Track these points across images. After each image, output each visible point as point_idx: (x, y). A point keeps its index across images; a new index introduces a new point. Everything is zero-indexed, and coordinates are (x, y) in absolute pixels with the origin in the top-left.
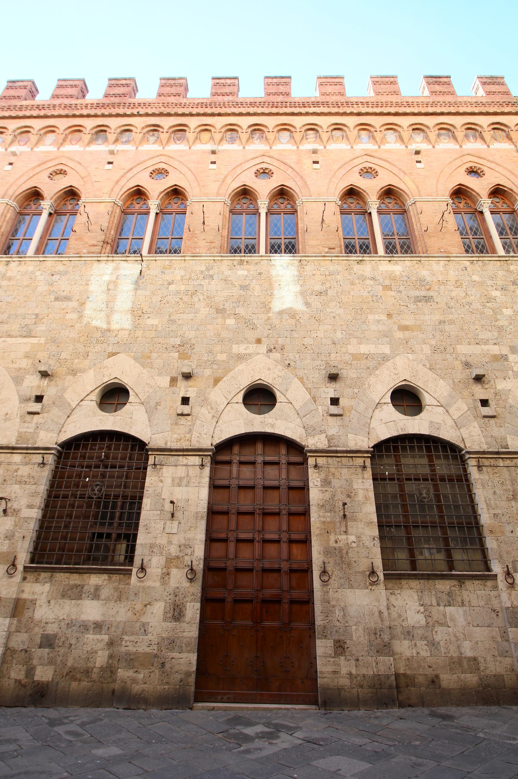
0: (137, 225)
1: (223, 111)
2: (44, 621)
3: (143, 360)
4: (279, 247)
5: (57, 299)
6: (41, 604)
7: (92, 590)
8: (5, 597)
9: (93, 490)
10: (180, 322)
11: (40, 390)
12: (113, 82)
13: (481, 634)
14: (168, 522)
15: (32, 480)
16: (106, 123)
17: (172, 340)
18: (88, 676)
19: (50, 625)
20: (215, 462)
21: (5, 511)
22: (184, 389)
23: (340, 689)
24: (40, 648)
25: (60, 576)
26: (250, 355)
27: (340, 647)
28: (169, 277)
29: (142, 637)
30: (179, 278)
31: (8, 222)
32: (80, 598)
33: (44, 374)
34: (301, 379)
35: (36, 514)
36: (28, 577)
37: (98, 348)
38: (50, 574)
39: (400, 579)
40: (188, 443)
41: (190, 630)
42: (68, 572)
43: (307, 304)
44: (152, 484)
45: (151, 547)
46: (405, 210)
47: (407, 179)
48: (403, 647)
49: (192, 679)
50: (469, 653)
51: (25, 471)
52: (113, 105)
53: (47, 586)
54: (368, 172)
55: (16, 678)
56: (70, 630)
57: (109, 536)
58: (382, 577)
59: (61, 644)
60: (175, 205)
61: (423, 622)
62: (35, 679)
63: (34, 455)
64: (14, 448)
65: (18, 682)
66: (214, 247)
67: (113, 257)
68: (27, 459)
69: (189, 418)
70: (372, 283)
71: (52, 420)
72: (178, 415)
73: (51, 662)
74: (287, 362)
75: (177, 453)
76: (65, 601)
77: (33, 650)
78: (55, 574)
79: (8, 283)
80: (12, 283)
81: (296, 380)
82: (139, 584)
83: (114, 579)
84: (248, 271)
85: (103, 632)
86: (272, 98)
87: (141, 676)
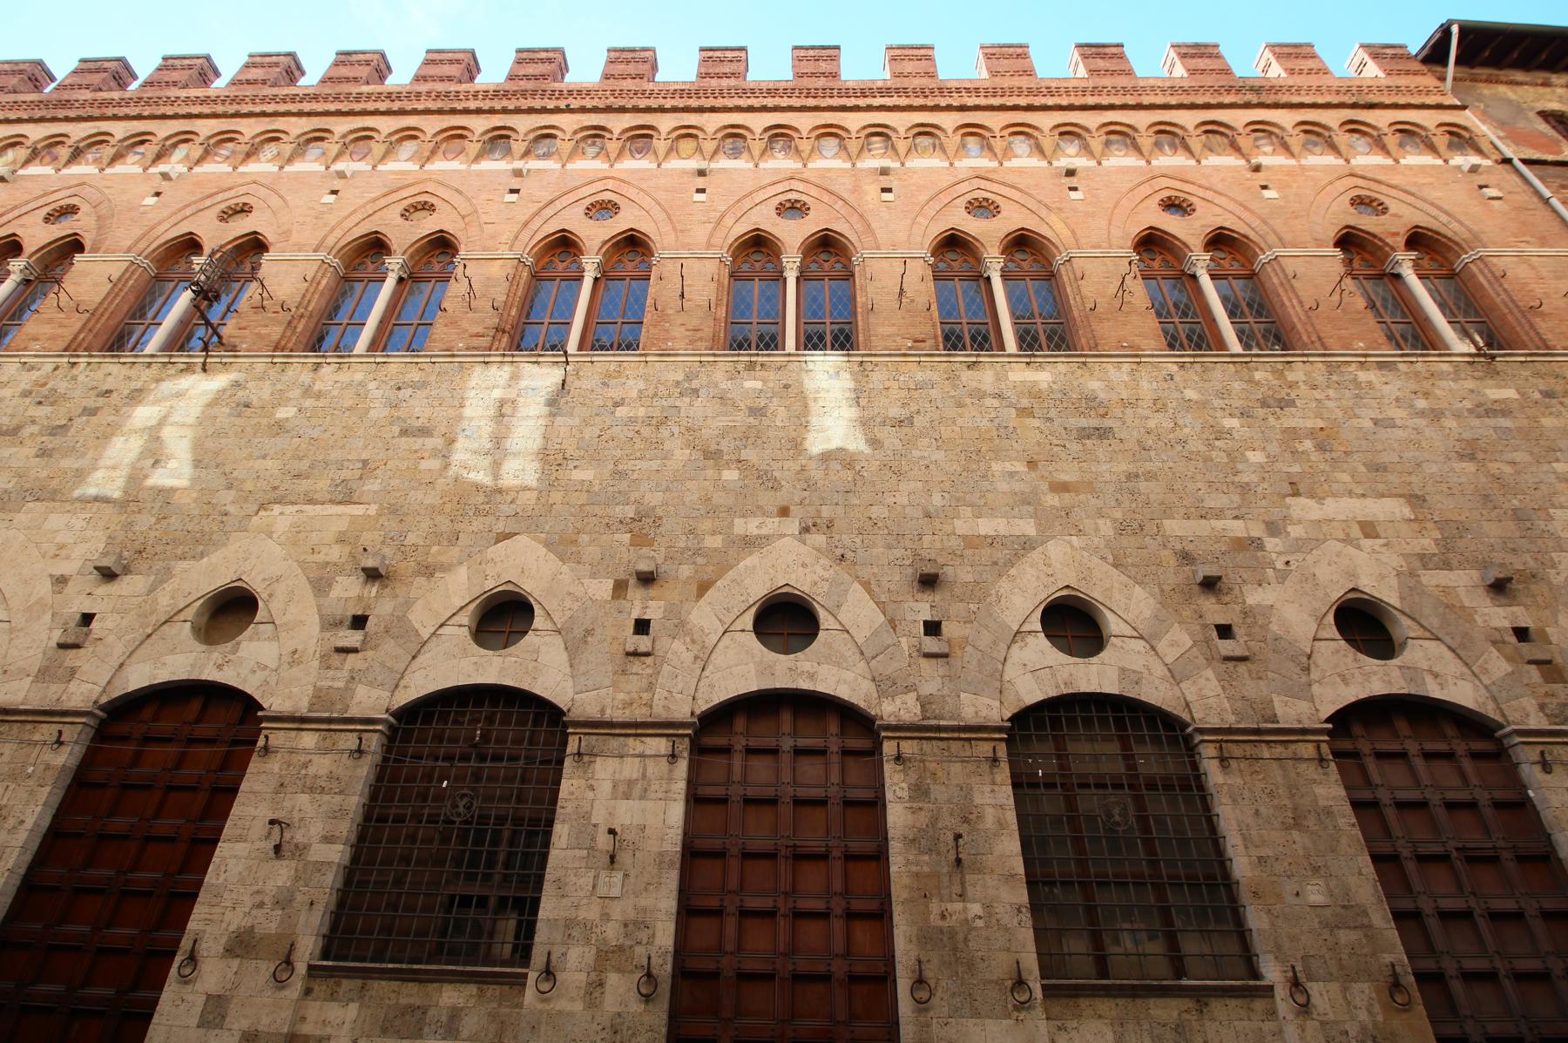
3: (563, 547)
5: (404, 432)
7: (444, 1019)
12: (525, 55)
14: (603, 874)
16: (103, 129)
17: (619, 508)
20: (699, 750)
21: (278, 849)
22: (639, 604)
25: (379, 987)
26: (767, 537)
30: (634, 394)
31: (322, 294)
33: (372, 575)
34: (866, 585)
35: (337, 854)
37: (478, 524)
38: (359, 982)
39: (1077, 996)
40: (645, 710)
43: (874, 443)
45: (567, 926)
47: (1053, 219)
51: (322, 765)
53: (353, 1010)
54: (982, 207)
66: (701, 339)
69: (649, 660)
70: (996, 403)
71: (383, 665)
72: (628, 654)
74: (839, 552)
81: (856, 585)
82: (540, 1006)
84: (765, 382)
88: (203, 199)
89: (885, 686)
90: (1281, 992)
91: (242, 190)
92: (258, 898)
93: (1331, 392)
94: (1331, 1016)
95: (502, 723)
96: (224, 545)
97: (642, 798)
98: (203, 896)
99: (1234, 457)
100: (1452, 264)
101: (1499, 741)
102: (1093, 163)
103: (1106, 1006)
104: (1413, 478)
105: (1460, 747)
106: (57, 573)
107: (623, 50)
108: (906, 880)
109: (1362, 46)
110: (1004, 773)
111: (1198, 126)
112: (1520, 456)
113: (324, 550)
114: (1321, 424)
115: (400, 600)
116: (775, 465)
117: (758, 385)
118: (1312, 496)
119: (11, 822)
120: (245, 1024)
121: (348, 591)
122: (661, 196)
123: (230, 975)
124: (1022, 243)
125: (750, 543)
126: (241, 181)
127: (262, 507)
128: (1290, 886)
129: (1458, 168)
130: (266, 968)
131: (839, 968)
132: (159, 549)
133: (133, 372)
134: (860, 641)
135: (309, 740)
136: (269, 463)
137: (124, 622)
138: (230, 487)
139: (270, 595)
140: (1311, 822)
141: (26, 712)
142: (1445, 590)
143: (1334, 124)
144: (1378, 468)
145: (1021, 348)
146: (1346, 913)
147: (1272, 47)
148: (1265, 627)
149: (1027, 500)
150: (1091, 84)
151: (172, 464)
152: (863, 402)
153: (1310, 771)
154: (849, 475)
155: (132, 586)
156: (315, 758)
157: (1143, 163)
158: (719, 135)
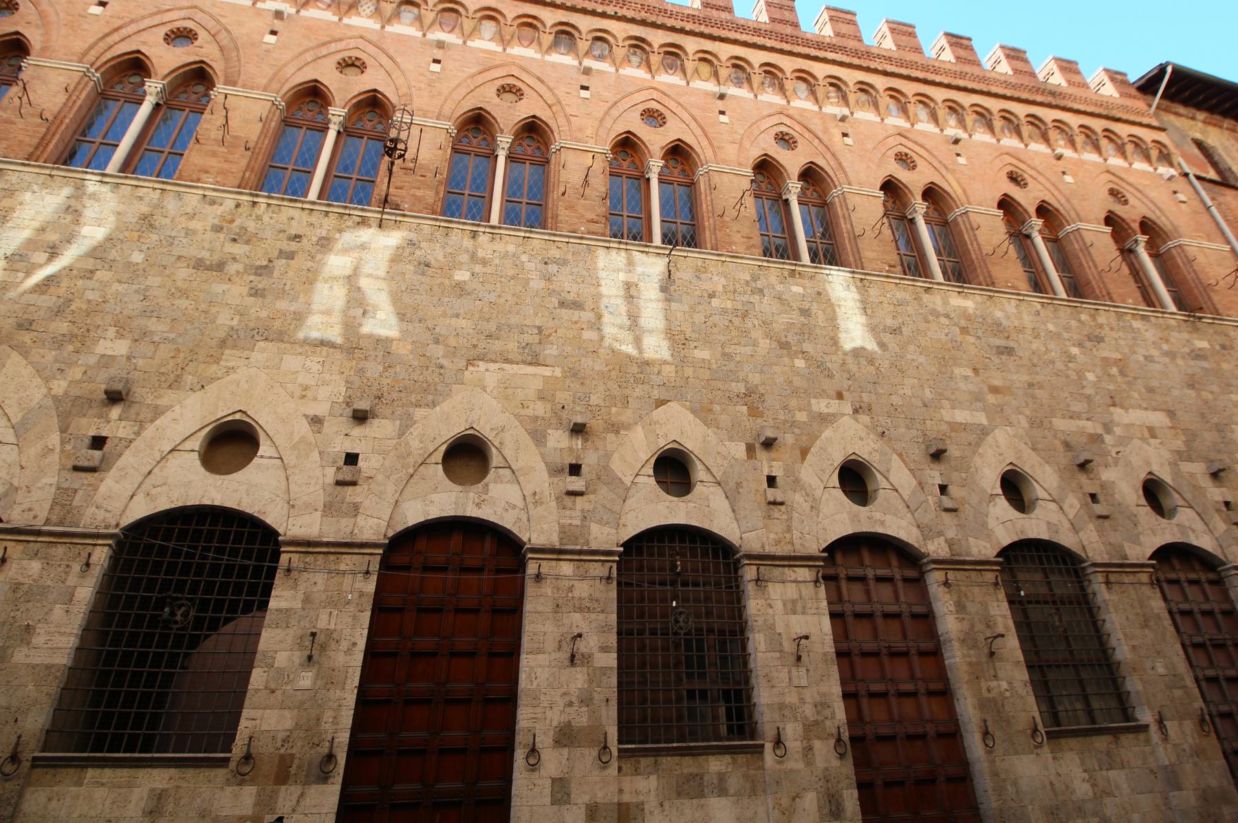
0: (184, 130)
1: (724, 33)
3: (703, 413)
4: (459, 207)
5: (562, 304)
7: (715, 781)
9: (677, 621)
14: (794, 670)
15: (596, 605)
16: (928, 93)
17: (734, 384)
22: (768, 464)
25: (667, 762)
26: (833, 415)
28: (707, 286)
30: (720, 289)
32: (701, 795)
34: (900, 455)
35: (611, 660)
37: (639, 391)
38: (652, 759)
39: (1059, 737)
40: (789, 547)
43: (882, 345)
45: (780, 709)
47: (949, 177)
51: (583, 589)
54: (653, 117)
58: (615, 753)
60: (307, 113)
61: (1091, 794)
64: (560, 552)
66: (753, 246)
69: (783, 508)
70: (946, 321)
72: (770, 503)
74: (880, 430)
78: (659, 759)
79: (485, 270)
80: (489, 270)
81: (895, 457)
82: (778, 767)
84: (804, 288)
88: (318, 46)
89: (927, 531)
90: (1153, 728)
91: (352, 43)
92: (567, 699)
93: (1121, 334)
94: (1177, 741)
95: (692, 556)
96: (449, 395)
97: (803, 613)
98: (523, 700)
99: (1080, 375)
100: (1158, 247)
101: (1219, 573)
103: (1073, 742)
104: (1168, 399)
105: (1203, 577)
106: (311, 412)
107: (899, 24)
108: (965, 668)
109: (1002, 47)
110: (1001, 595)
112: (1215, 388)
114: (1119, 356)
115: (601, 452)
116: (827, 358)
118: (1122, 407)
119: (344, 645)
120: (586, 798)
121: (558, 440)
122: (696, 113)
123: (564, 761)
124: (678, 152)
125: (825, 419)
126: (349, 34)
127: (470, 362)
128: (1148, 664)
129: (1161, 175)
130: (591, 753)
132: (395, 395)
133: (314, 219)
134: (906, 498)
135: (566, 568)
136: (462, 323)
137: (387, 462)
138: (437, 342)
139: (501, 443)
140: (1152, 623)
141: (328, 544)
142: (1192, 475)
143: (820, 76)
144: (1151, 390)
145: (663, 242)
146: (1174, 681)
147: (1057, 60)
148: (1112, 495)
149: (978, 397)
150: (769, 27)
151: (381, 315)
152: (869, 311)
153: (1146, 590)
154: (872, 369)
155: (381, 428)
157: (994, 141)
158: (479, 15)
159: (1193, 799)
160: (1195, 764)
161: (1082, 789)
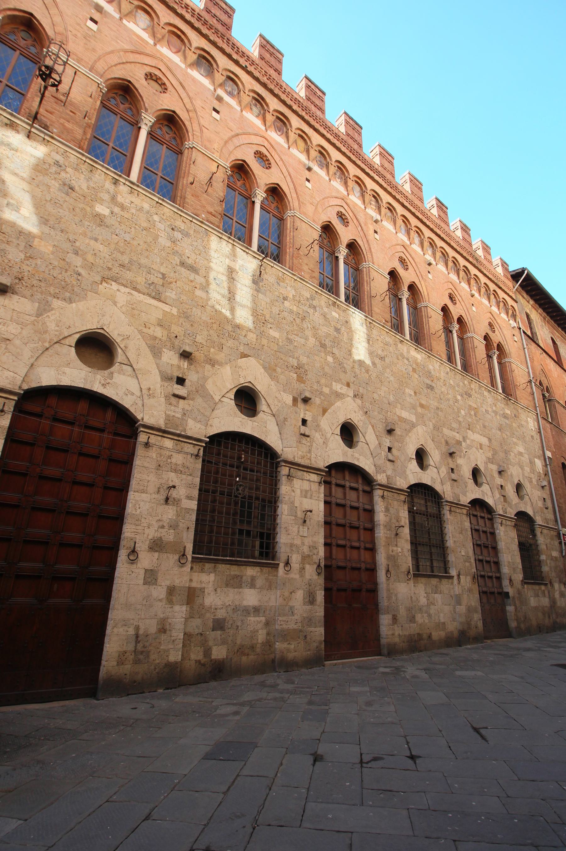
2: (213, 607)
3: (270, 370)
6: (209, 592)
7: (249, 580)
8: (178, 585)
9: (238, 490)
10: (295, 344)
11: (181, 371)
13: (447, 609)
14: (301, 527)
16: (347, 165)
18: (254, 651)
19: (218, 610)
21: (167, 499)
22: (303, 412)
23: (395, 644)
24: (213, 631)
25: (222, 567)
27: (395, 619)
29: (290, 617)
32: (240, 587)
33: (186, 355)
34: (373, 426)
35: (194, 505)
36: (194, 567)
38: (213, 565)
40: (309, 461)
41: (319, 611)
42: (228, 564)
43: (374, 364)
44: (287, 492)
45: (291, 546)
46: (181, 151)
48: (419, 618)
49: (323, 646)
50: (442, 620)
51: (178, 459)
52: (205, 23)
53: (212, 577)
55: (196, 658)
56: (236, 614)
57: (248, 533)
59: (230, 626)
61: (426, 603)
62: (212, 658)
63: (186, 444)
64: (164, 432)
65: (198, 662)
67: (234, 241)
68: (179, 447)
69: (308, 439)
71: (198, 410)
72: (301, 434)
73: (224, 642)
74: (365, 410)
75: (303, 469)
76: (229, 589)
77: (208, 633)
78: (217, 565)
82: (285, 576)
83: (264, 571)
85: (261, 615)
86: (207, 16)
87: (292, 647)
90: (456, 578)
102: (117, 16)
103: (423, 580)
110: (406, 507)
111: (198, 48)
113: (152, 328)
117: (337, 316)
120: (168, 583)
123: (155, 560)
124: (170, 120)
128: (459, 550)
131: (363, 566)
135: (168, 443)
139: (126, 347)
143: (315, 143)
156: (174, 454)
159: (464, 610)
160: (468, 595)
161: (423, 601)
